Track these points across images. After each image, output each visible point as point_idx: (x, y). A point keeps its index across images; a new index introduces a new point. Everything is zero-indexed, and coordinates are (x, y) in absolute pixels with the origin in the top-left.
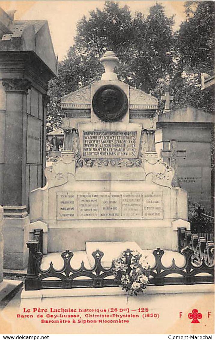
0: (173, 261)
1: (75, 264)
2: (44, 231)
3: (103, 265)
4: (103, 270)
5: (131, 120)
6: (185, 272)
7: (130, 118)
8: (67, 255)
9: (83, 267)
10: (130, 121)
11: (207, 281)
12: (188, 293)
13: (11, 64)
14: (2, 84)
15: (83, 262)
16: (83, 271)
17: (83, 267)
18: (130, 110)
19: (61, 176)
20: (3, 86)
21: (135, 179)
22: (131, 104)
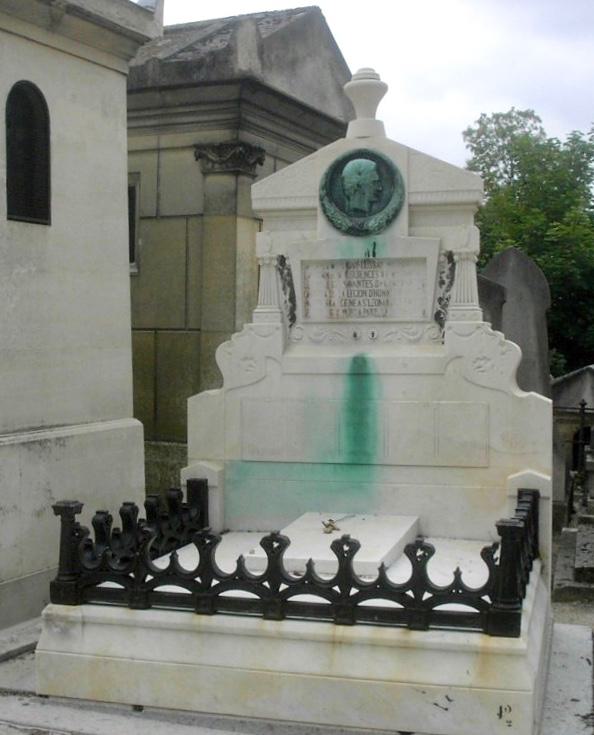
0: (458, 574)
1: (439, 575)
2: (542, 495)
3: (357, 570)
4: (287, 580)
5: (413, 229)
6: (429, 599)
7: (410, 225)
8: (346, 548)
9: (457, 581)
10: (409, 231)
11: (315, 615)
12: (385, 646)
13: (205, 111)
14: (195, 155)
15: (458, 569)
16: (240, 578)
17: (457, 581)
18: (410, 205)
19: (251, 362)
20: (197, 160)
21: (389, 371)
22: (412, 190)
